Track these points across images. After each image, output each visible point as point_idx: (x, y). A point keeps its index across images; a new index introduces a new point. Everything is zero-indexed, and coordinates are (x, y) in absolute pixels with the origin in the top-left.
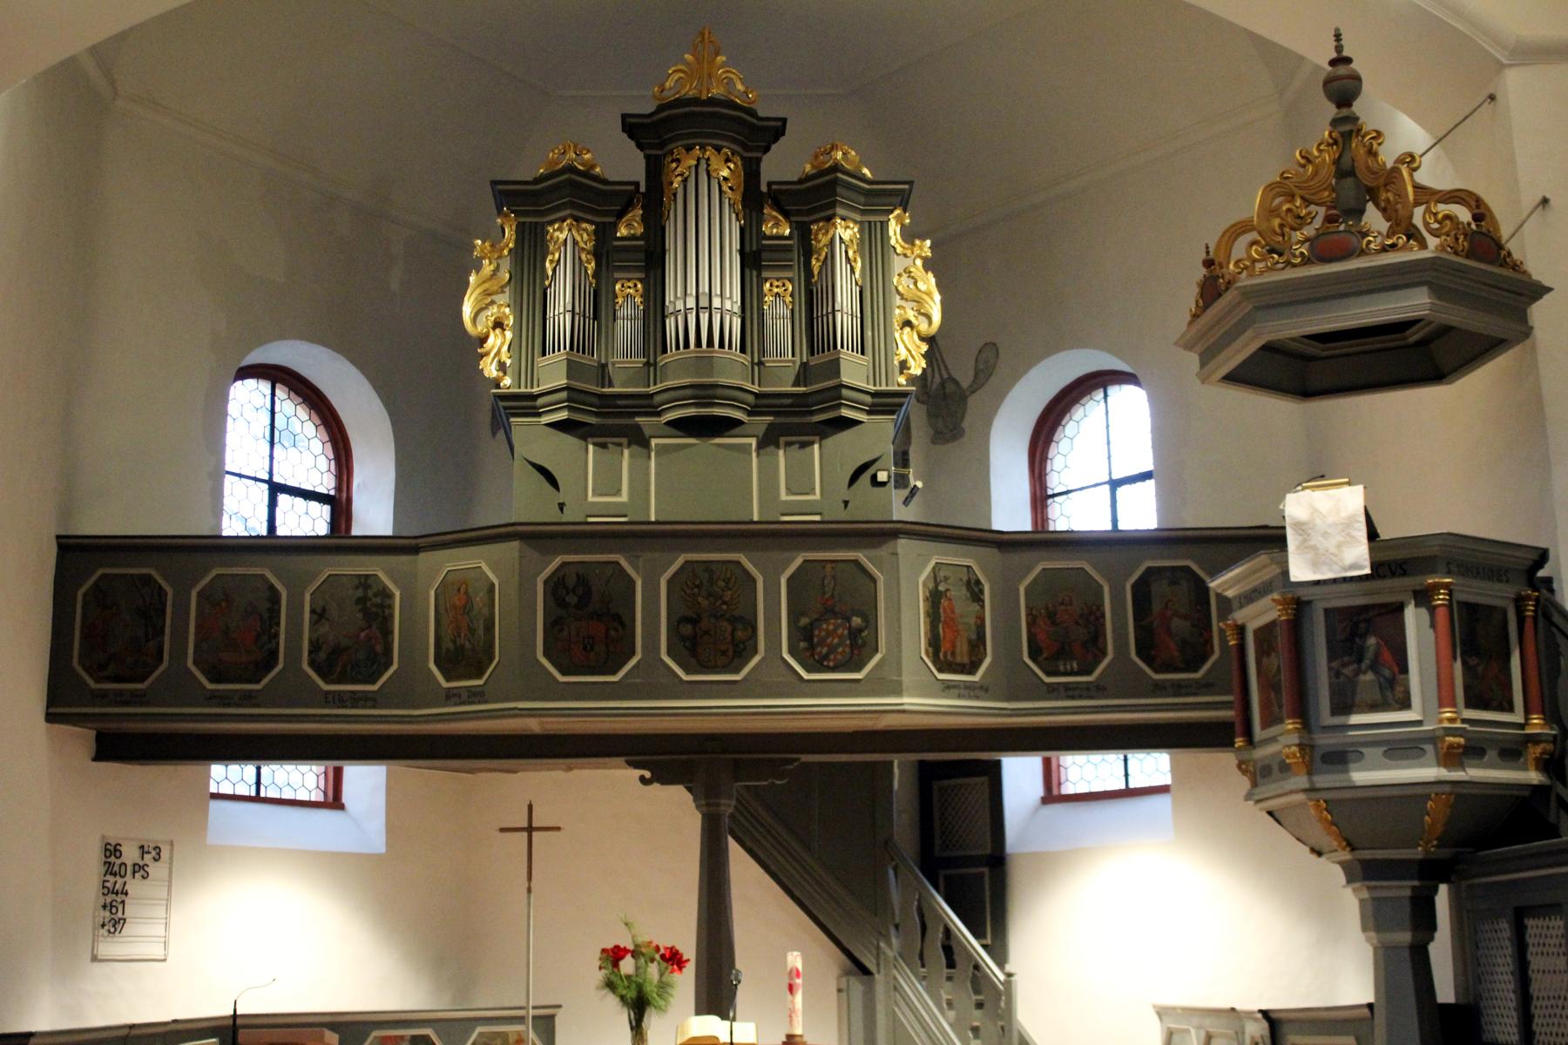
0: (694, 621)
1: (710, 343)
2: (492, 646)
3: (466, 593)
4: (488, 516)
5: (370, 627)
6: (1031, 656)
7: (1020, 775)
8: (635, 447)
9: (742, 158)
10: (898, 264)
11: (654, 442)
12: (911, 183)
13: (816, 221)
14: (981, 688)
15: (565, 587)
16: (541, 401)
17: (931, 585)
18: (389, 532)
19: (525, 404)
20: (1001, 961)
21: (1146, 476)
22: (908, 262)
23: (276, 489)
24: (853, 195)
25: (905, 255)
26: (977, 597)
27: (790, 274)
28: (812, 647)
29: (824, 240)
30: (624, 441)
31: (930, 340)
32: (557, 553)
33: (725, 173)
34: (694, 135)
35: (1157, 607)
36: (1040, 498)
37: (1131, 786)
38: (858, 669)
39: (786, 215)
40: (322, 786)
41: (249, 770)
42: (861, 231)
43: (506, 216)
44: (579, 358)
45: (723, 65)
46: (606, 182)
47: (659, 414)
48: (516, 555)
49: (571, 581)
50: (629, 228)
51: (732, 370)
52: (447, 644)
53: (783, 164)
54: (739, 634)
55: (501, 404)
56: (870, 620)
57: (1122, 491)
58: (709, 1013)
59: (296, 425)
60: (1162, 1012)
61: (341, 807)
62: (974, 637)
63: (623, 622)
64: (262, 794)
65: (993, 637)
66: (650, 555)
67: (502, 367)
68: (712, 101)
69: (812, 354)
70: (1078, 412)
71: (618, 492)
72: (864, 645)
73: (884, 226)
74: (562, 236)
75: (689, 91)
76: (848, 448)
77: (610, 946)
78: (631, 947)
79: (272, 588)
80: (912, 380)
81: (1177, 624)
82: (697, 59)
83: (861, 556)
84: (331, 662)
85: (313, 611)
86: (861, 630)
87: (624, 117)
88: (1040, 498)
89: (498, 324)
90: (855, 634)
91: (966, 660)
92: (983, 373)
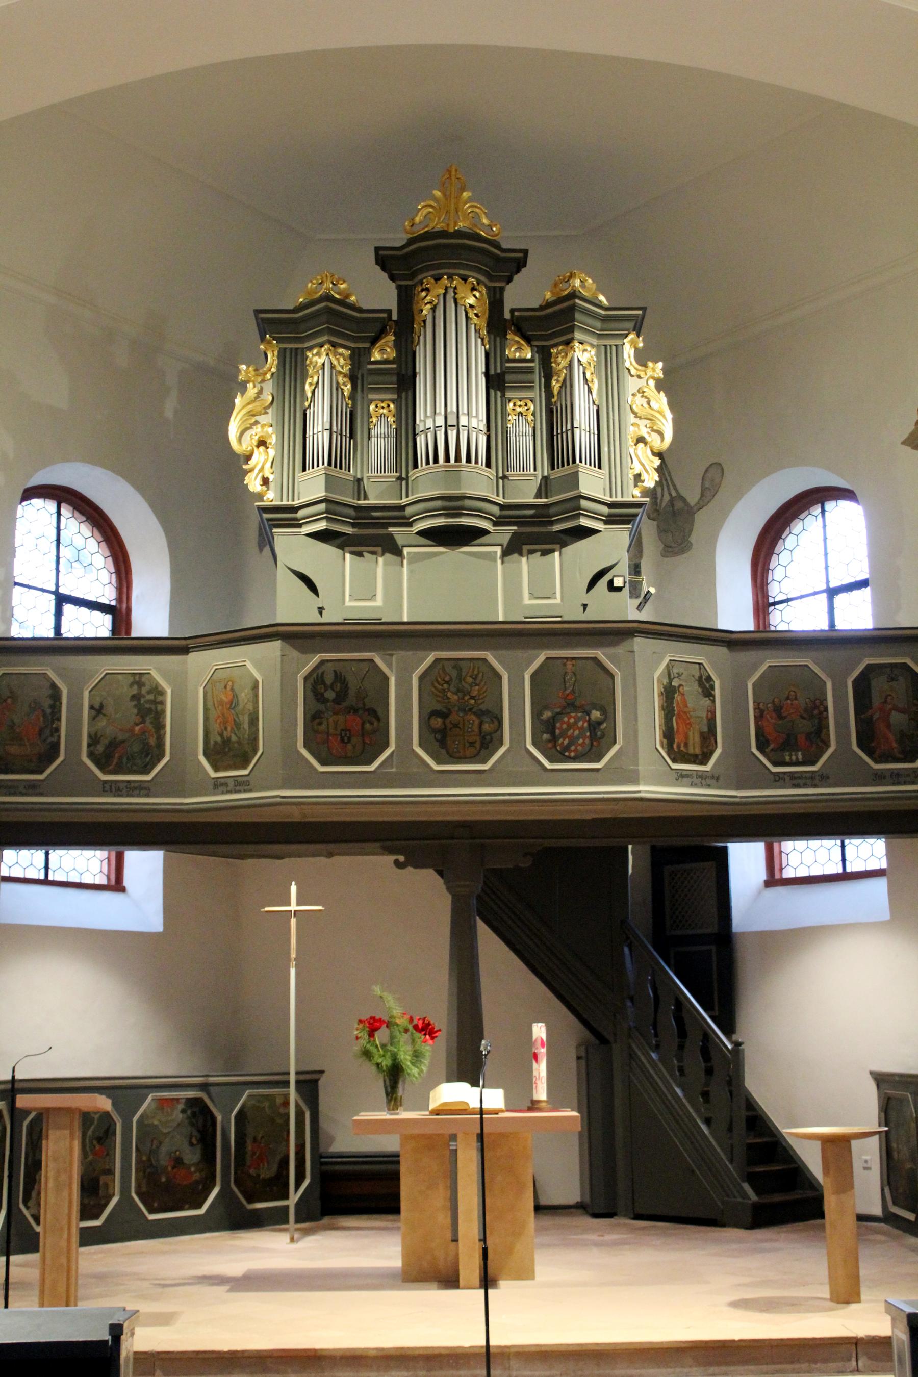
0: (444, 715)
1: (458, 458)
2: (256, 739)
3: (232, 690)
4: (254, 619)
5: (143, 722)
6: (759, 748)
7: (745, 860)
8: (388, 555)
9: (487, 287)
10: (632, 385)
11: (406, 551)
12: (644, 309)
13: (556, 345)
14: (713, 777)
15: (323, 683)
16: (301, 513)
17: (666, 681)
18: (165, 634)
19: (285, 516)
20: (729, 1028)
21: (864, 584)
22: (642, 383)
23: (62, 600)
24: (589, 321)
25: (639, 377)
26: (708, 692)
27: (530, 394)
28: (554, 739)
29: (564, 363)
30: (379, 549)
31: (660, 455)
32: (316, 651)
33: (471, 301)
34: (439, 267)
35: (876, 701)
36: (763, 605)
37: (848, 870)
38: (598, 760)
39: (528, 340)
40: (105, 870)
41: (38, 855)
42: (598, 354)
43: (269, 342)
44: (335, 472)
45: (469, 200)
46: (360, 310)
47: (410, 525)
48: (279, 653)
49: (329, 679)
50: (383, 353)
51: (478, 482)
52: (215, 738)
53: (524, 293)
54: (486, 727)
55: (266, 516)
56: (608, 712)
57: (839, 599)
58: (460, 1079)
59: (79, 541)
60: (881, 1079)
61: (122, 890)
62: (705, 729)
63: (375, 715)
64: (50, 878)
65: (723, 728)
66: (403, 653)
67: (266, 481)
68: (459, 234)
69: (553, 468)
70: (797, 526)
71: (373, 597)
72: (603, 736)
73: (619, 348)
74: (320, 361)
75: (438, 225)
76: (584, 556)
77: (365, 1017)
78: (386, 1019)
79: (54, 686)
80: (646, 492)
81: (896, 718)
82: (444, 195)
83: (599, 654)
84: (108, 754)
85: (91, 707)
86: (599, 723)
87: (377, 249)
88: (763, 605)
89: (262, 443)
90: (594, 726)
91: (698, 751)
92: (709, 491)
